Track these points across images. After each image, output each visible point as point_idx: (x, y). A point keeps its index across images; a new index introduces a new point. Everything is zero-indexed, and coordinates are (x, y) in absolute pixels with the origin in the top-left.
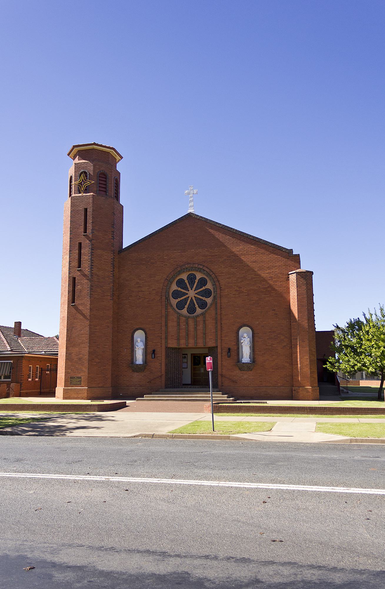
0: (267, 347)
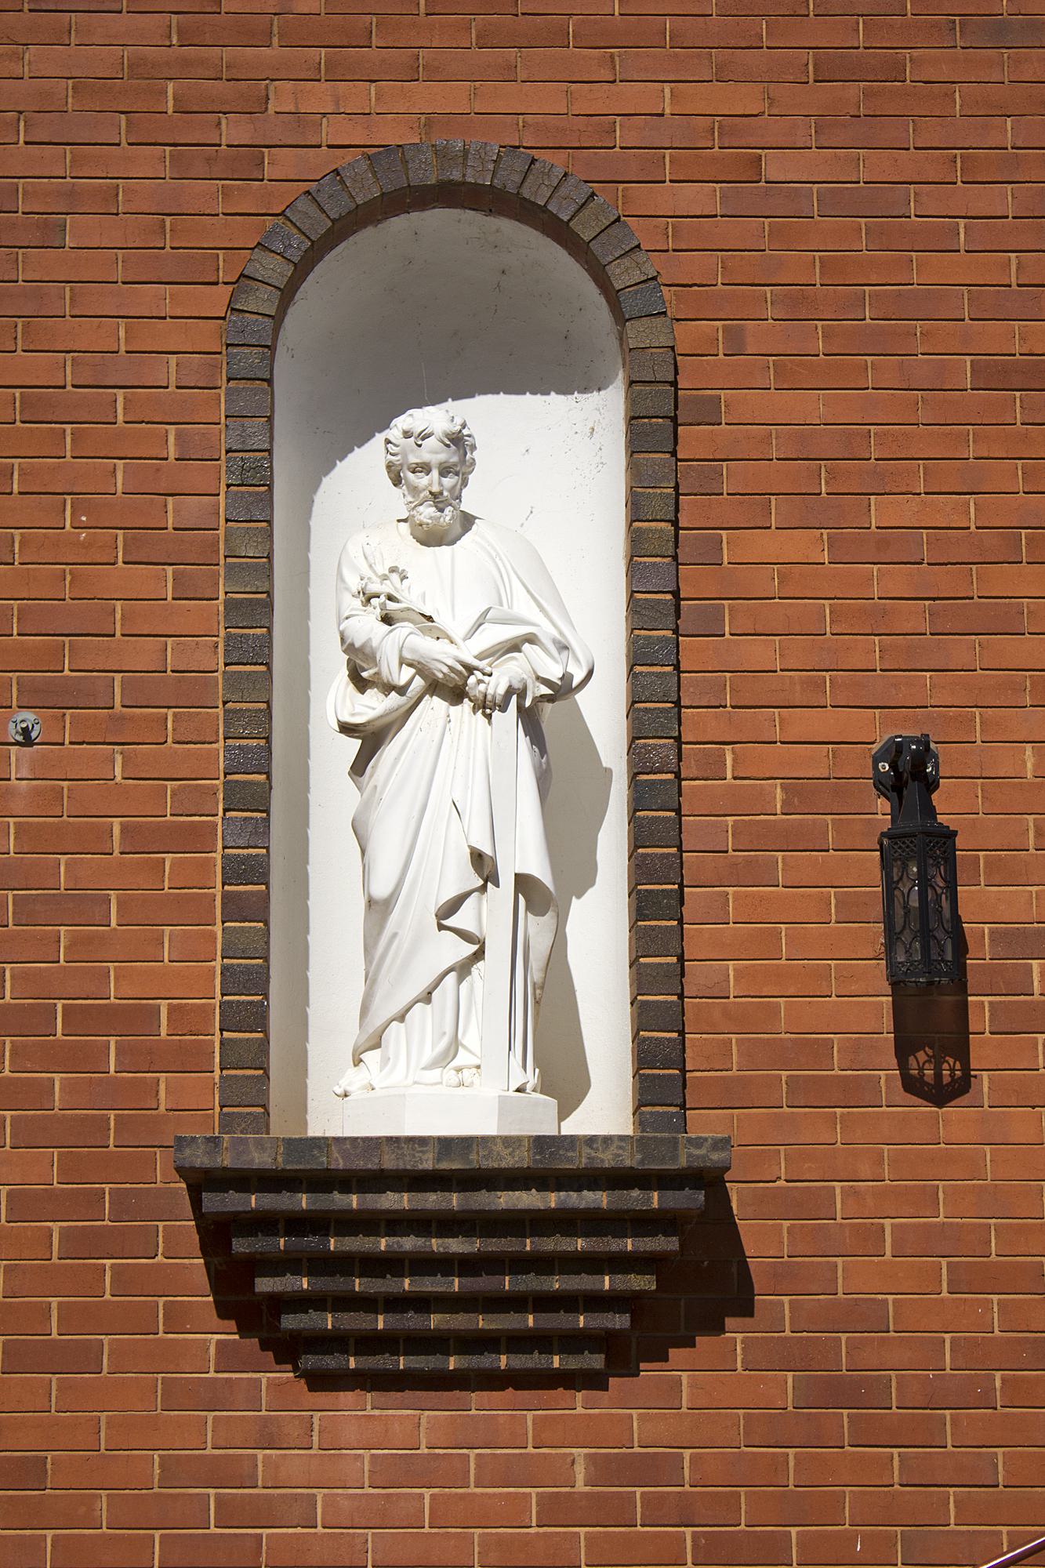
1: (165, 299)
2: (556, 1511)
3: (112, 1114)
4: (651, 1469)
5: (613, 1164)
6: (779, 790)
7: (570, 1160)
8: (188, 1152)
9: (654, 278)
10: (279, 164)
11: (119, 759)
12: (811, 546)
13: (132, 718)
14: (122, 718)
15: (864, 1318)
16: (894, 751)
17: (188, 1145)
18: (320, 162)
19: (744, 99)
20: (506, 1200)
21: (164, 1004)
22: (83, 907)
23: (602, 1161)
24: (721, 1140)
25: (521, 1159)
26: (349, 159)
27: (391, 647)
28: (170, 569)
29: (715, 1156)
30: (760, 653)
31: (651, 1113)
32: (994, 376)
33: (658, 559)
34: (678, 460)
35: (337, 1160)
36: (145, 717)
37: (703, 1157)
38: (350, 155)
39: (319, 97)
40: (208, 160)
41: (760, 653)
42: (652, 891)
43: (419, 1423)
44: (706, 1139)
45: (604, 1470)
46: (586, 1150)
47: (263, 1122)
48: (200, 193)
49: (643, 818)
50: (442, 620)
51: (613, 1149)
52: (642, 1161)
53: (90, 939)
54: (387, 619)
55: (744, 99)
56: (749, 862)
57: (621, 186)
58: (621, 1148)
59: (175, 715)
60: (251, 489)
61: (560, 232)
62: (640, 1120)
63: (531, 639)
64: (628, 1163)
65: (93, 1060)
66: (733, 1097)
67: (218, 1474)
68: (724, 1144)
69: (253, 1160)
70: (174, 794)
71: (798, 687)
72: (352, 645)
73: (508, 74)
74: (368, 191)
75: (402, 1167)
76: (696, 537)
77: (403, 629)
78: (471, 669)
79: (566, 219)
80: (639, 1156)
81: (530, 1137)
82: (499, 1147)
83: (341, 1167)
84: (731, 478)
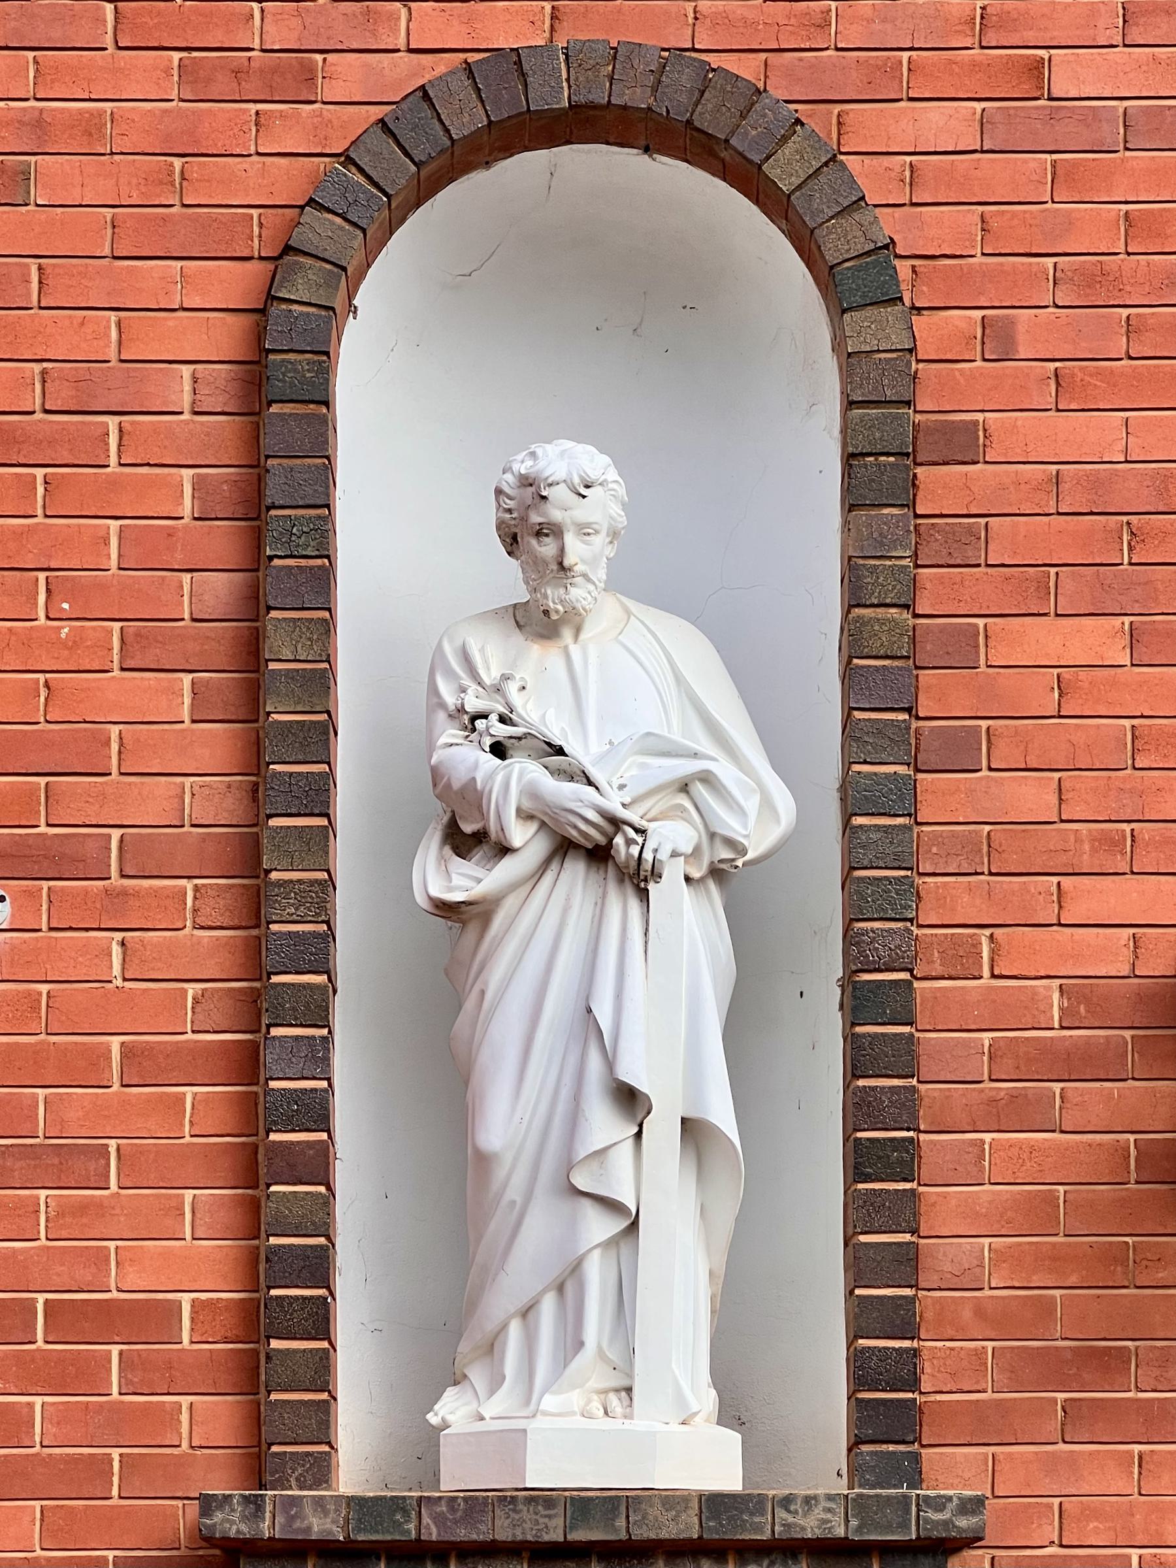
1: (158, 278)
3: (115, 1453)
5: (818, 1533)
6: (1056, 996)
7: (759, 1528)
8: (218, 1516)
9: (886, 247)
10: (346, 76)
11: (116, 950)
12: (1099, 641)
13: (137, 894)
14: (124, 893)
17: (220, 1507)
18: (401, 74)
21: (186, 1299)
23: (803, 1529)
24: (970, 1499)
26: (441, 69)
28: (187, 679)
29: (963, 1522)
30: (1033, 797)
31: (872, 1453)
33: (887, 662)
34: (917, 516)
35: (428, 1527)
36: (155, 893)
37: (946, 1523)
38: (442, 65)
40: (236, 72)
41: (1033, 797)
42: (877, 1140)
44: (950, 1499)
46: (781, 1514)
48: (223, 120)
49: (864, 1035)
50: (580, 752)
51: (818, 1513)
52: (859, 1529)
53: (83, 1208)
54: (499, 750)
56: (1013, 1097)
57: (837, 108)
58: (829, 1510)
59: (196, 889)
60: (303, 562)
61: (748, 179)
62: (856, 1471)
63: (364, 231)
64: (840, 1532)
65: (87, 1377)
66: (987, 1427)
68: (974, 1505)
69: (309, 1529)
70: (196, 1001)
71: (1087, 847)
72: (448, 785)
74: (467, 119)
75: (520, 1538)
76: (943, 629)
78: (616, 823)
79: (756, 158)
80: (854, 1523)
81: (701, 1496)
82: (655, 1512)
83: (434, 1538)
84: (1006, 540)
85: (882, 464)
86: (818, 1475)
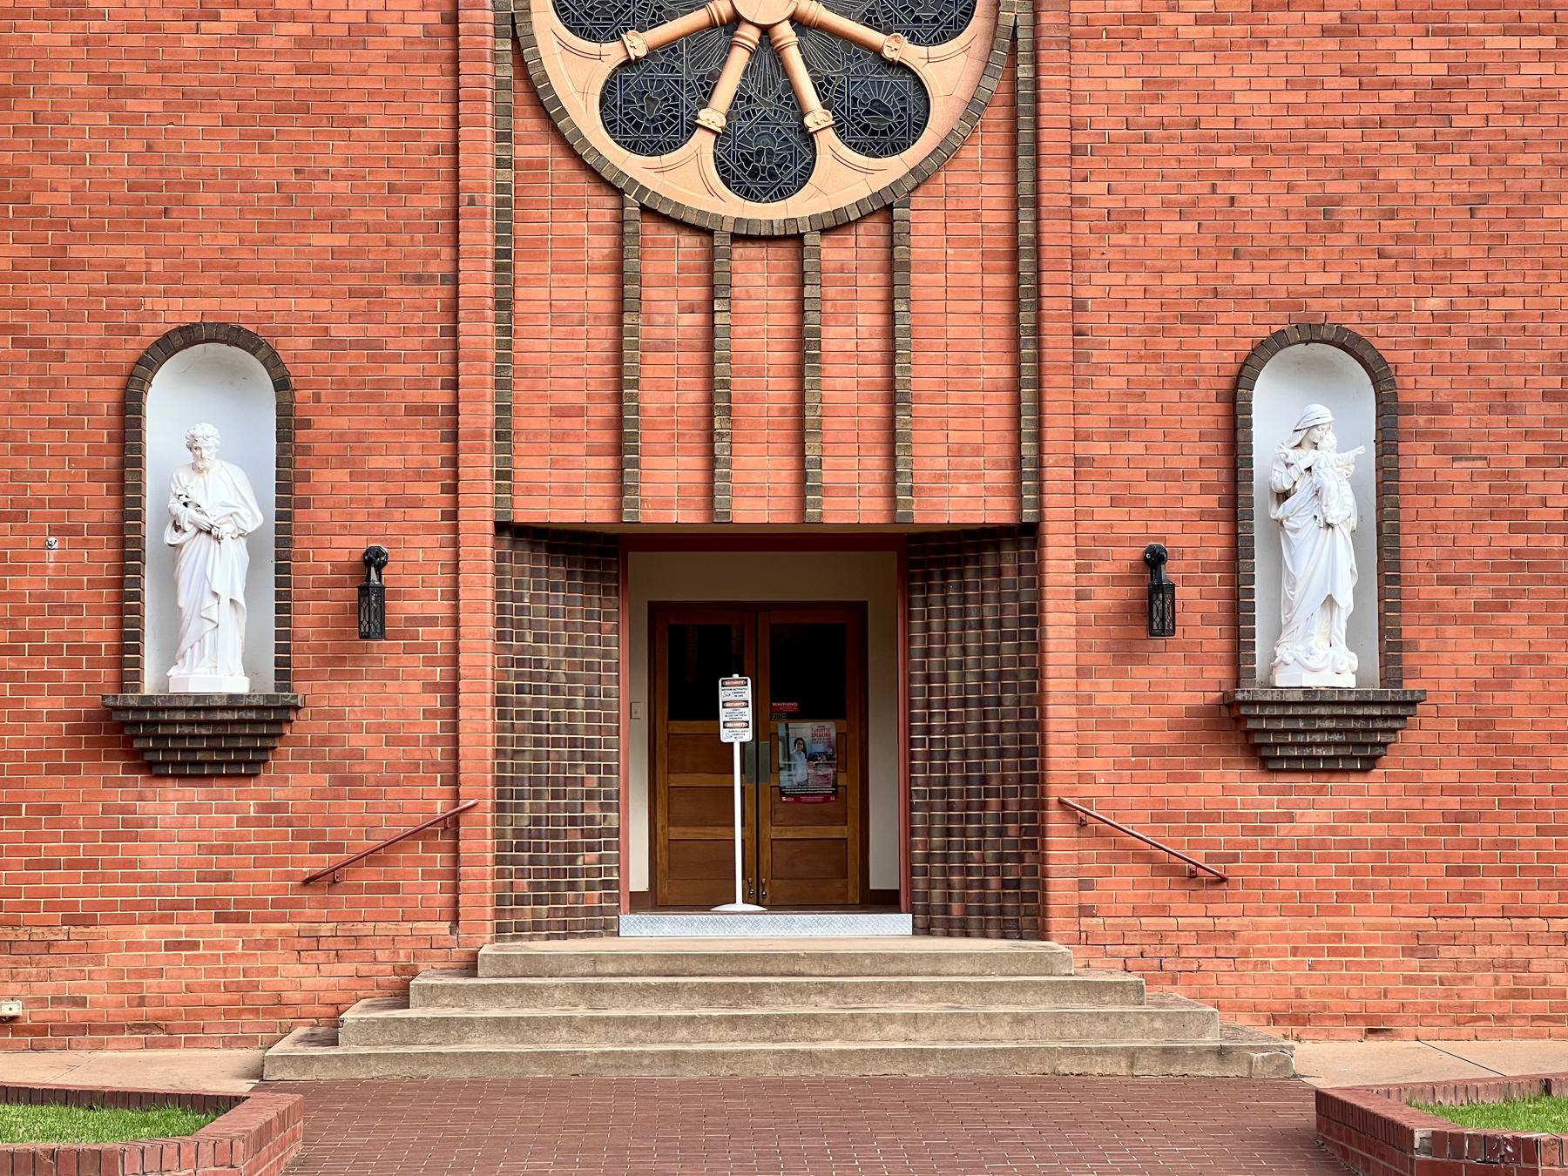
0: (1519, 541)
2: (243, 822)
4: (277, 808)
15: (357, 755)
16: (1152, 550)
19: (323, 305)
20: (219, 716)
22: (74, 609)
25: (224, 702)
27: (186, 516)
32: (1203, 515)
39: (160, 304)
43: (195, 793)
45: (263, 808)
47: (137, 688)
50: (204, 507)
55: (323, 305)
65: (78, 664)
67: (123, 810)
73: (234, 295)
77: (191, 510)
85: (1387, 443)
86: (1374, 686)
